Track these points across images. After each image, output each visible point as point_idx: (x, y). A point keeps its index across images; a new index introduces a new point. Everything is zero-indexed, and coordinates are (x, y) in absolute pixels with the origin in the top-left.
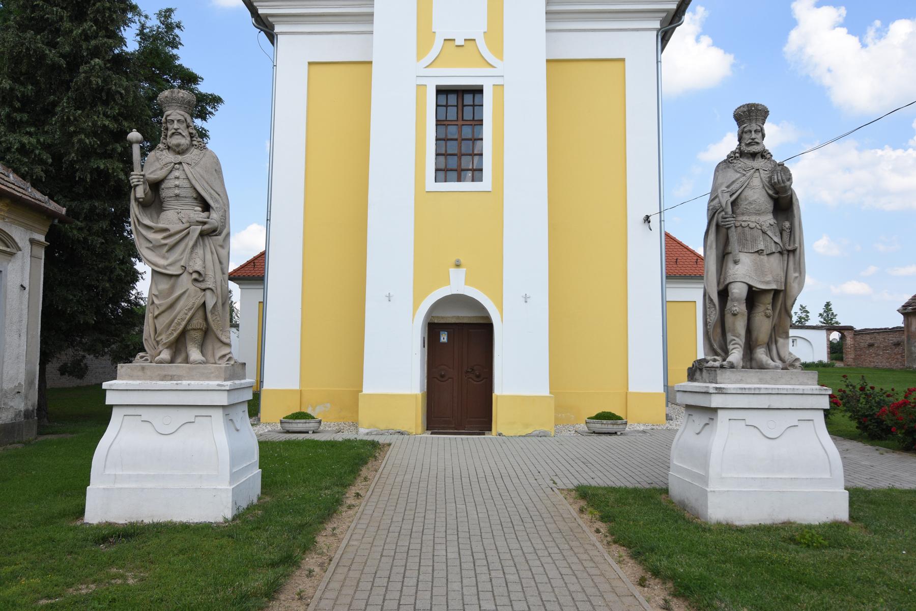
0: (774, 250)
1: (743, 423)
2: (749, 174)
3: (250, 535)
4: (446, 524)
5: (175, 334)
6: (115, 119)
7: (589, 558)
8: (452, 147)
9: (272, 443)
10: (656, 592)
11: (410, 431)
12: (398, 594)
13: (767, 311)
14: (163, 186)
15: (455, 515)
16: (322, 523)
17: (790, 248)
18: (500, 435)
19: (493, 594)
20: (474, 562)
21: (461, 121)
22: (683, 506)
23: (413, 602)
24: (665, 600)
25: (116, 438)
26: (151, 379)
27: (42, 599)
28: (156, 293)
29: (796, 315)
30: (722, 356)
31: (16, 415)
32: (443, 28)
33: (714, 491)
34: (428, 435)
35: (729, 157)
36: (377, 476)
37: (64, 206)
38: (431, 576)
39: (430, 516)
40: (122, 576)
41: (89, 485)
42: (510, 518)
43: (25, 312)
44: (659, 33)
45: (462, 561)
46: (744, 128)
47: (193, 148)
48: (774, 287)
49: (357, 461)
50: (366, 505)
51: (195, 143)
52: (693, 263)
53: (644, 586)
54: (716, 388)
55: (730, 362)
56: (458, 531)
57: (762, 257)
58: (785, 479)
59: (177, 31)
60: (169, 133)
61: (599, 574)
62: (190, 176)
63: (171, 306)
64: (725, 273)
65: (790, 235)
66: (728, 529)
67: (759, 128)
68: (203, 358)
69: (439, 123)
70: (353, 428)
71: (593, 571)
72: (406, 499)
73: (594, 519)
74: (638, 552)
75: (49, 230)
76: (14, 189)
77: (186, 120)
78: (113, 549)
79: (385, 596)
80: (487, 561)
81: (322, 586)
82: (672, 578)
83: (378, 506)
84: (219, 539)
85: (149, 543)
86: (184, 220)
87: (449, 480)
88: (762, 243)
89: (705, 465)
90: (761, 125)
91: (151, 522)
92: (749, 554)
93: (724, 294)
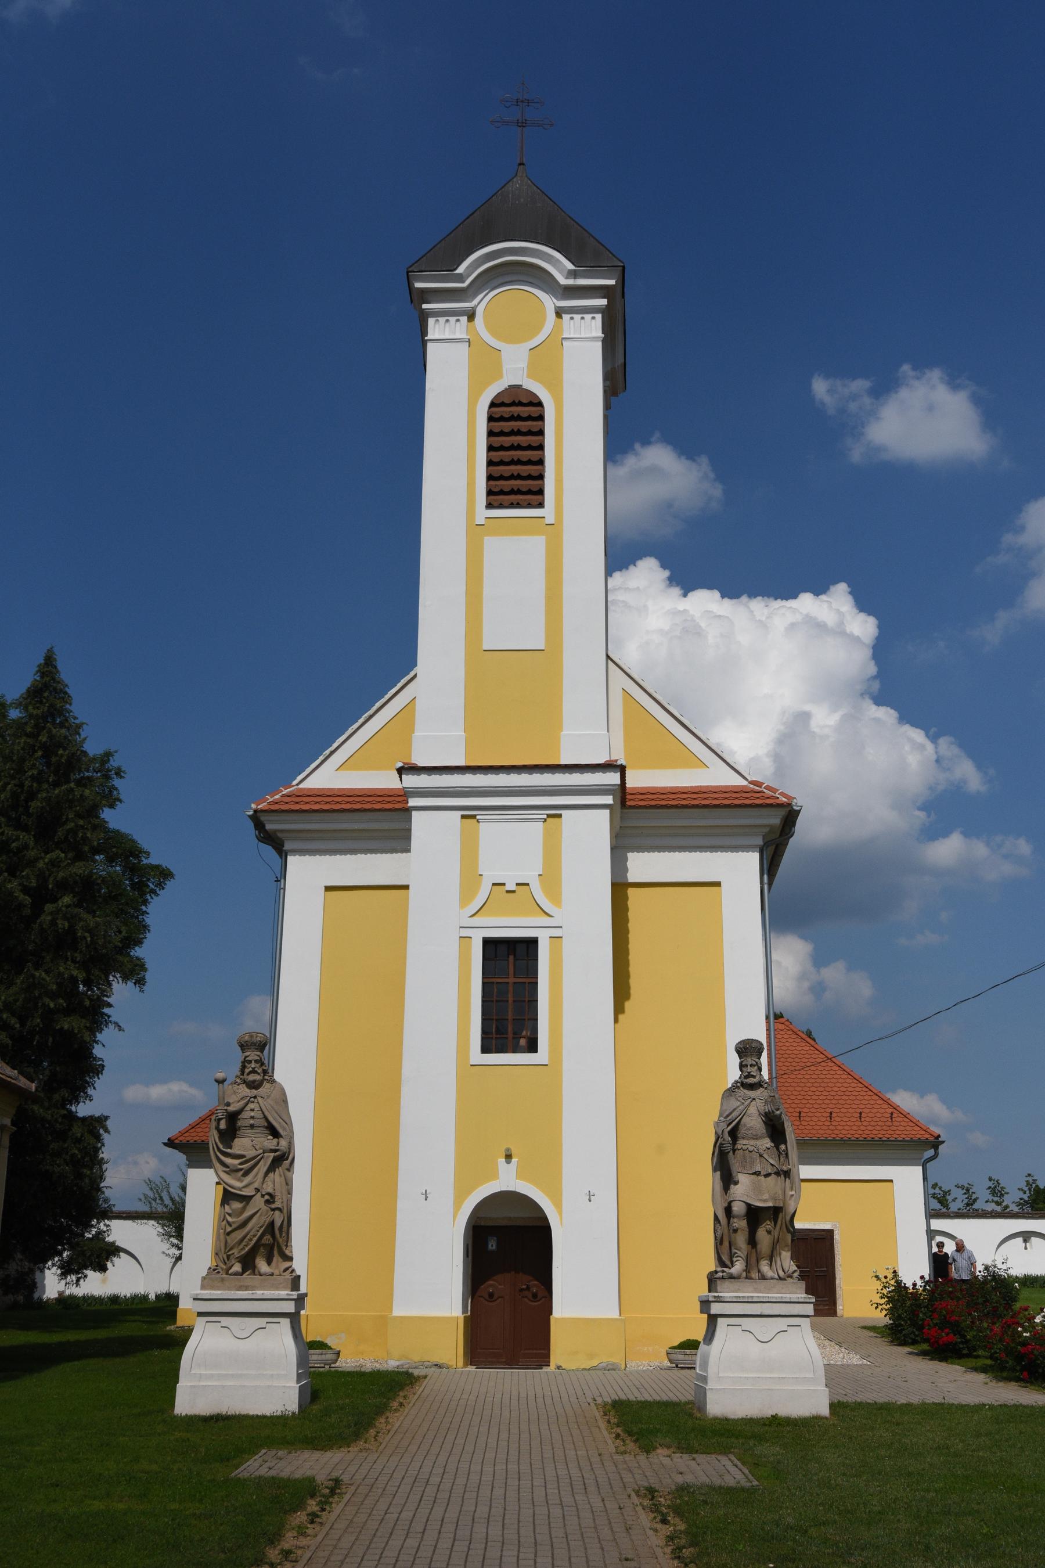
11: (450, 1363)
17: (785, 1169)
26: (229, 1289)
28: (230, 1212)
32: (490, 873)
34: (472, 1369)
48: (770, 1204)
54: (715, 1297)
62: (264, 1108)
67: (754, 1063)
86: (257, 1147)
88: (759, 1165)
90: (757, 1060)
93: (728, 1210)
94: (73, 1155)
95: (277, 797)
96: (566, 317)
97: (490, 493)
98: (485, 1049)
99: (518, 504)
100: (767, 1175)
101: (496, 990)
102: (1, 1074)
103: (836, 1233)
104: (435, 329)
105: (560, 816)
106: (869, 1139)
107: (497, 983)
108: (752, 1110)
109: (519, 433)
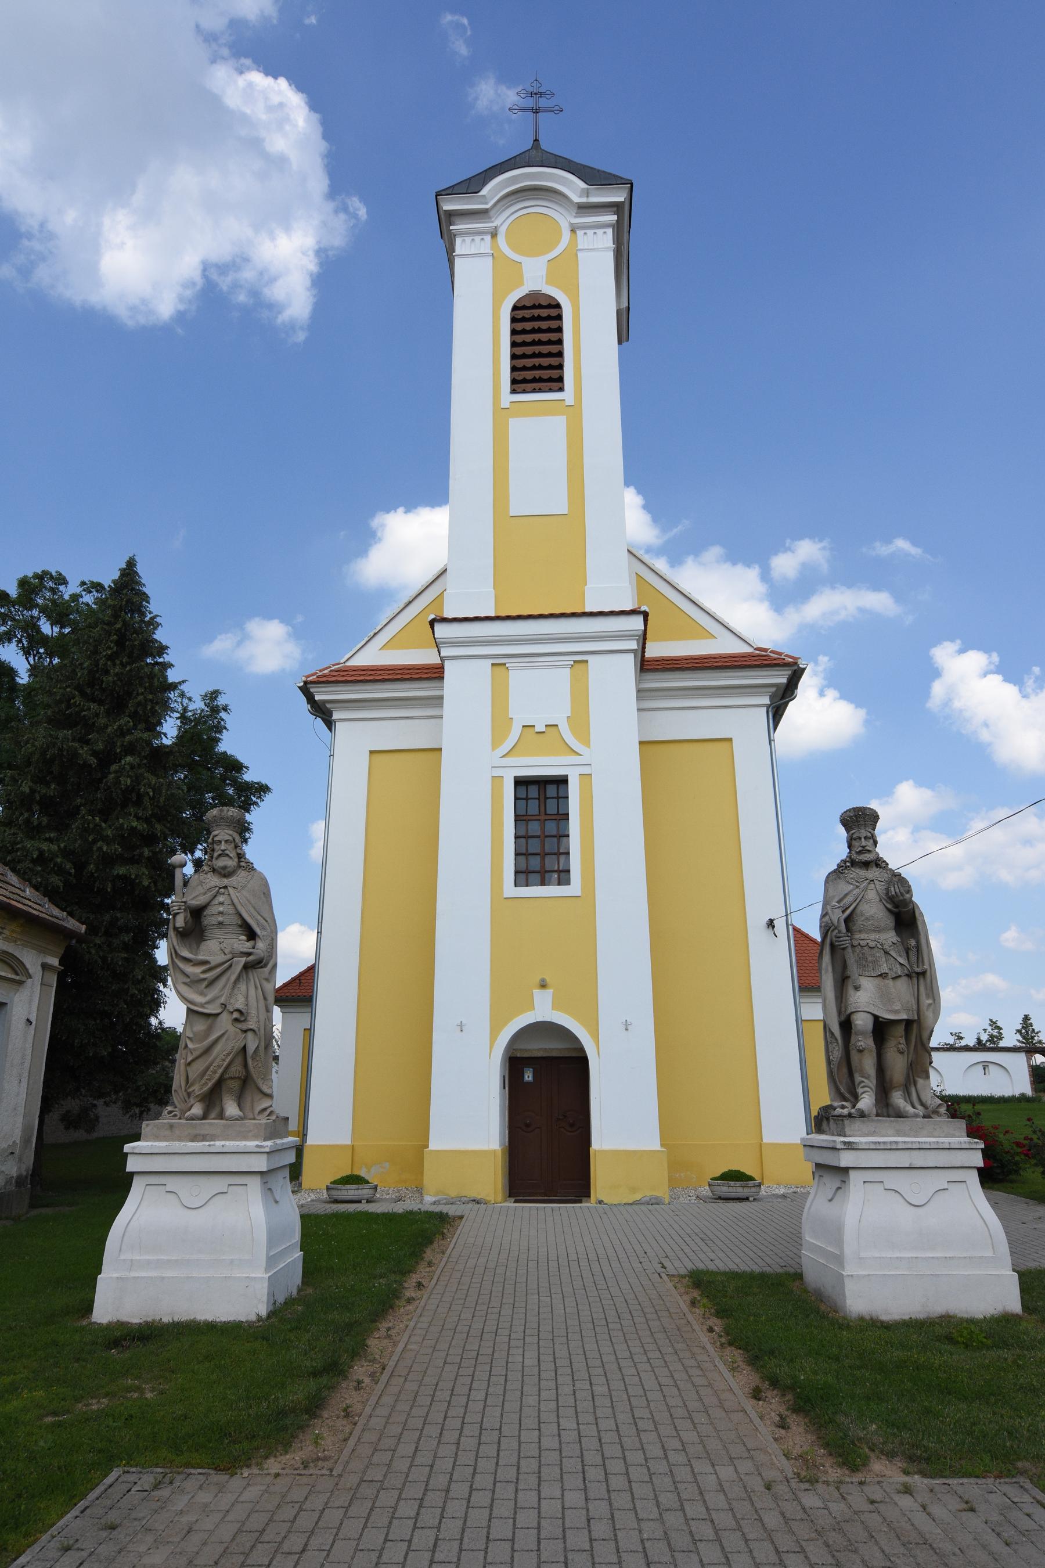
0: (900, 973)
1: (880, 1187)
2: (862, 886)
3: (288, 1337)
4: (525, 1322)
5: (210, 1085)
6: (147, 820)
7: (697, 1365)
8: (534, 846)
9: (317, 1217)
10: (773, 1407)
11: (488, 1198)
12: (462, 1410)
13: (900, 1046)
14: (205, 913)
15: (537, 1310)
16: (374, 1321)
17: (918, 970)
18: (600, 1203)
19: (576, 1411)
20: (556, 1371)
21: (543, 816)
22: (820, 1296)
23: (479, 1420)
24: (780, 1416)
25: (135, 1212)
26: (180, 1139)
27: (47, 1415)
28: (191, 1036)
29: (985, 1032)
30: (851, 1102)
31: (6, 1183)
32: (521, 714)
33: (852, 1276)
34: (510, 1204)
35: (839, 866)
36: (445, 1259)
37: (83, 924)
38: (503, 1388)
39: (507, 1311)
40: (138, 1389)
41: (100, 1274)
42: (605, 1314)
43: (29, 1052)
44: (770, 710)
45: (542, 1368)
46: (853, 834)
47: (240, 870)
48: (904, 1016)
49: (420, 1240)
50: (429, 1298)
51: (242, 864)
53: (759, 1400)
54: (845, 1143)
55: (859, 1109)
56: (539, 1331)
57: (887, 981)
58: (938, 1258)
59: (223, 714)
60: (216, 854)
61: (706, 1384)
62: (236, 901)
63: (208, 1050)
64: (846, 1001)
65: (918, 953)
66: (872, 1325)
67: (869, 835)
68: (241, 1114)
69: (518, 818)
70: (417, 1195)
71: (699, 1381)
72: (478, 1290)
73: (707, 1315)
74: (757, 1356)
75: (65, 951)
76: (30, 907)
77: (234, 840)
78: (127, 1354)
79: (446, 1412)
80: (572, 1369)
81: (373, 1399)
82: (792, 1388)
83: (443, 1299)
84: (251, 1342)
85: (169, 1348)
86: (226, 951)
87: (532, 1265)
88: (885, 965)
89: (839, 1242)
90: (872, 831)
91: (171, 1321)
92: (892, 1357)
93: (846, 1025)
94: (133, 995)
97: (514, 382)
99: (540, 389)
102: (2, 895)
109: (540, 331)
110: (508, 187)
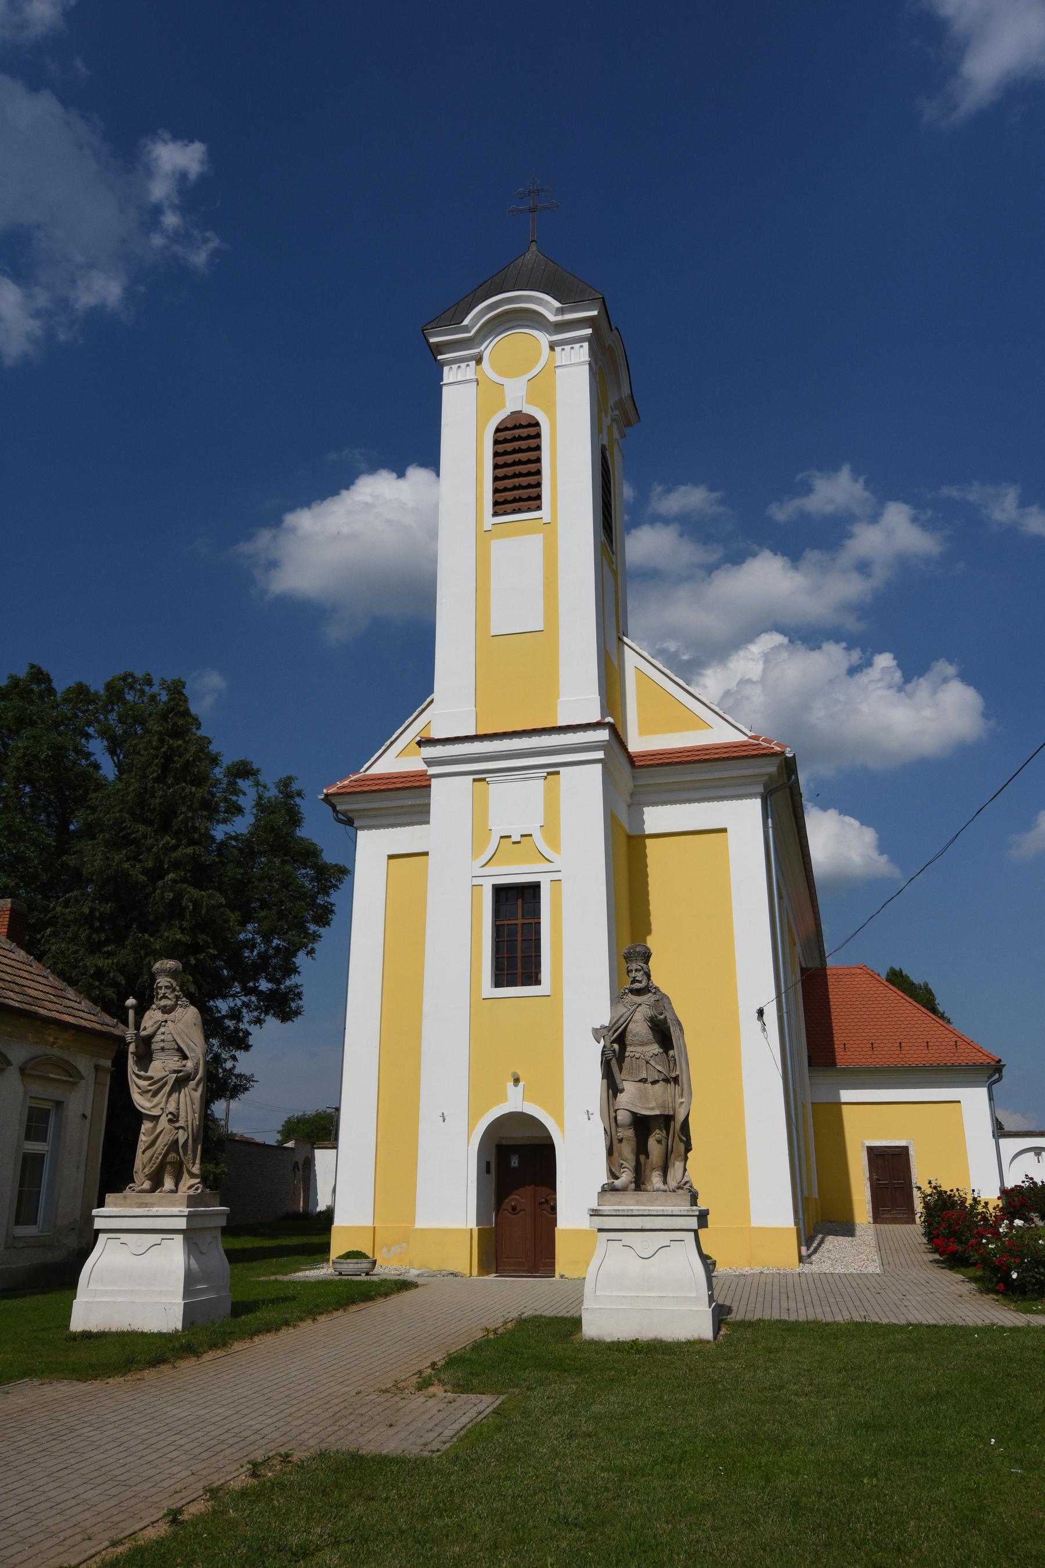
11: (465, 1272)
17: (673, 1075)
18: (562, 1278)
26: (131, 1206)
32: (499, 831)
33: (587, 1309)
48: (657, 1112)
52: (951, 1047)
57: (646, 1085)
58: (653, 1297)
59: (298, 800)
86: (166, 1069)
88: (645, 1072)
95: (346, 782)
96: (558, 349)
97: (496, 503)
98: (498, 983)
99: (519, 509)
100: (654, 1082)
101: (506, 931)
103: (911, 1149)
104: (449, 375)
105: (558, 773)
106: (935, 1065)
107: (508, 925)
108: (638, 1016)
109: (520, 451)
110: (488, 314)
